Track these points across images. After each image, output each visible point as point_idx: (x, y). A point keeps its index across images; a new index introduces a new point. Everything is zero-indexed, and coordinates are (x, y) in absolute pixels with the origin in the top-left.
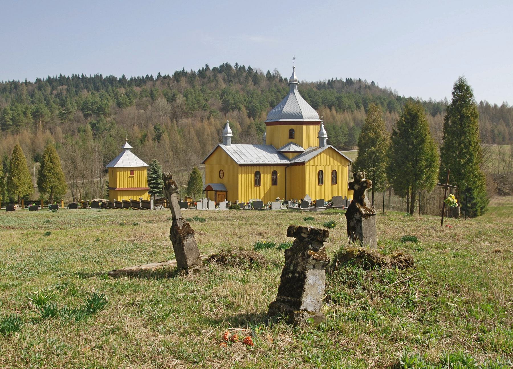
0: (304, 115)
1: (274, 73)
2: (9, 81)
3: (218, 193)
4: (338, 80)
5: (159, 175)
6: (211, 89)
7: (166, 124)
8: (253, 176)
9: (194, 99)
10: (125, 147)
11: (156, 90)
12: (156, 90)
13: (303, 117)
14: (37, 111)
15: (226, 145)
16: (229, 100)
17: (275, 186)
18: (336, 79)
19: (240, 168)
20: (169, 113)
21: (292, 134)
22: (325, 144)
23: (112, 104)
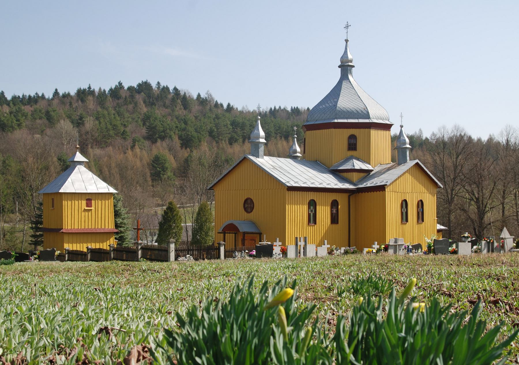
4: (282, 108)
8: (306, 207)
9: (108, 124)
10: (75, 160)
11: (54, 111)
12: (54, 111)
13: (371, 116)
15: (258, 156)
16: (156, 126)
17: (334, 226)
18: (280, 107)
19: (288, 194)
21: (352, 145)
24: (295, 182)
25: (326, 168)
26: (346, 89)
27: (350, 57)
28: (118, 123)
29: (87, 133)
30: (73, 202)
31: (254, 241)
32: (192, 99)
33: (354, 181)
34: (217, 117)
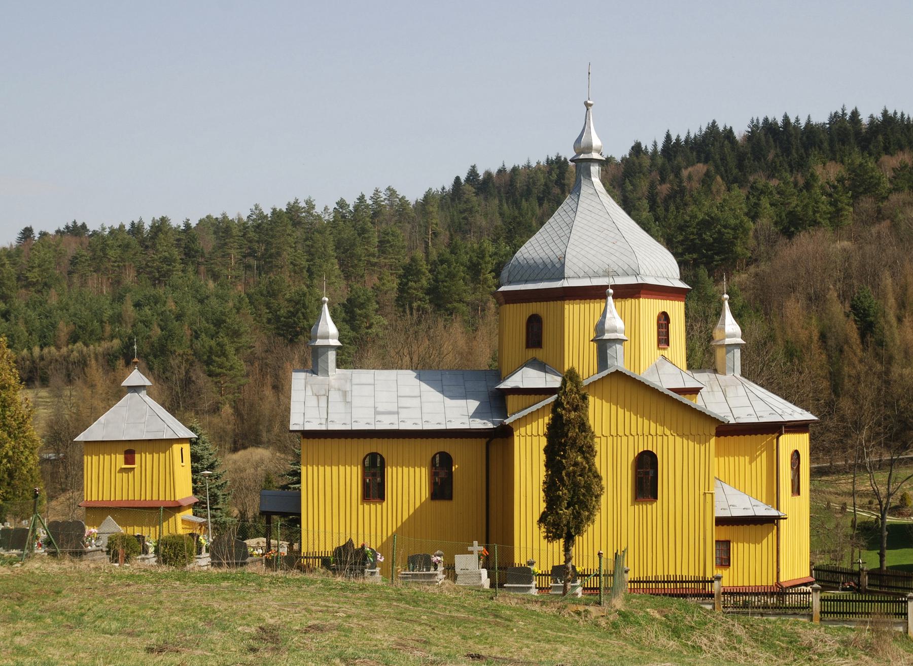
2: (501, 171)
10: (126, 383)
13: (567, 272)
17: (442, 505)
19: (306, 444)
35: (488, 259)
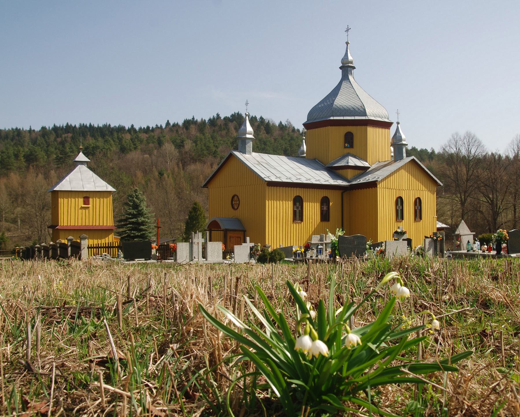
0: (368, 111)
1: (286, 123)
2: (12, 129)
3: (229, 234)
5: (140, 211)
6: (222, 136)
7: (172, 170)
8: (290, 204)
9: (203, 145)
10: (77, 159)
14: (31, 154)
15: (244, 152)
20: (176, 159)
21: (349, 139)
22: (405, 155)
23: (114, 148)
24: (277, 177)
25: (323, 166)
26: (345, 88)
27: (350, 58)
28: (211, 145)
29: (186, 153)
30: (70, 199)
31: (240, 239)
32: (274, 125)
33: (349, 178)
34: (292, 139)
35: (21, 153)
